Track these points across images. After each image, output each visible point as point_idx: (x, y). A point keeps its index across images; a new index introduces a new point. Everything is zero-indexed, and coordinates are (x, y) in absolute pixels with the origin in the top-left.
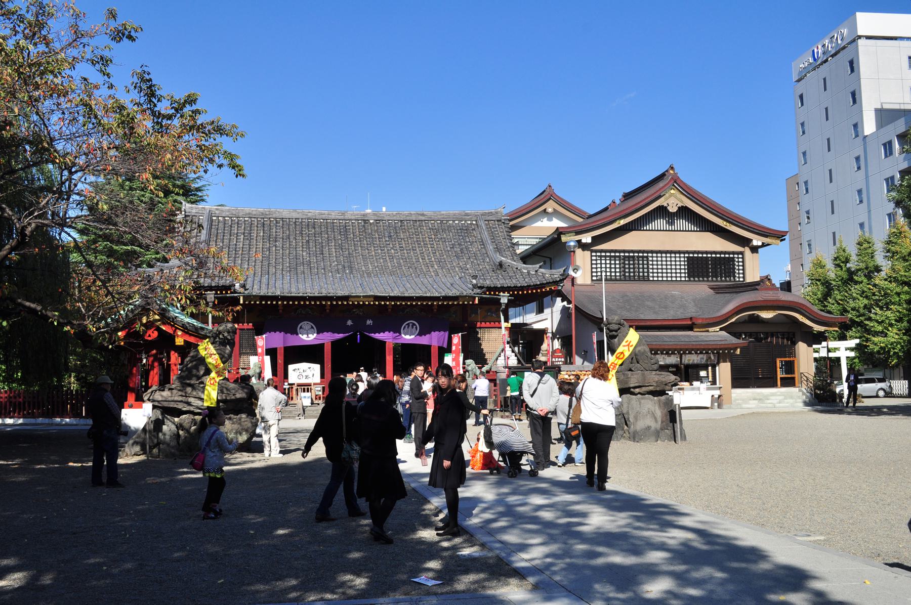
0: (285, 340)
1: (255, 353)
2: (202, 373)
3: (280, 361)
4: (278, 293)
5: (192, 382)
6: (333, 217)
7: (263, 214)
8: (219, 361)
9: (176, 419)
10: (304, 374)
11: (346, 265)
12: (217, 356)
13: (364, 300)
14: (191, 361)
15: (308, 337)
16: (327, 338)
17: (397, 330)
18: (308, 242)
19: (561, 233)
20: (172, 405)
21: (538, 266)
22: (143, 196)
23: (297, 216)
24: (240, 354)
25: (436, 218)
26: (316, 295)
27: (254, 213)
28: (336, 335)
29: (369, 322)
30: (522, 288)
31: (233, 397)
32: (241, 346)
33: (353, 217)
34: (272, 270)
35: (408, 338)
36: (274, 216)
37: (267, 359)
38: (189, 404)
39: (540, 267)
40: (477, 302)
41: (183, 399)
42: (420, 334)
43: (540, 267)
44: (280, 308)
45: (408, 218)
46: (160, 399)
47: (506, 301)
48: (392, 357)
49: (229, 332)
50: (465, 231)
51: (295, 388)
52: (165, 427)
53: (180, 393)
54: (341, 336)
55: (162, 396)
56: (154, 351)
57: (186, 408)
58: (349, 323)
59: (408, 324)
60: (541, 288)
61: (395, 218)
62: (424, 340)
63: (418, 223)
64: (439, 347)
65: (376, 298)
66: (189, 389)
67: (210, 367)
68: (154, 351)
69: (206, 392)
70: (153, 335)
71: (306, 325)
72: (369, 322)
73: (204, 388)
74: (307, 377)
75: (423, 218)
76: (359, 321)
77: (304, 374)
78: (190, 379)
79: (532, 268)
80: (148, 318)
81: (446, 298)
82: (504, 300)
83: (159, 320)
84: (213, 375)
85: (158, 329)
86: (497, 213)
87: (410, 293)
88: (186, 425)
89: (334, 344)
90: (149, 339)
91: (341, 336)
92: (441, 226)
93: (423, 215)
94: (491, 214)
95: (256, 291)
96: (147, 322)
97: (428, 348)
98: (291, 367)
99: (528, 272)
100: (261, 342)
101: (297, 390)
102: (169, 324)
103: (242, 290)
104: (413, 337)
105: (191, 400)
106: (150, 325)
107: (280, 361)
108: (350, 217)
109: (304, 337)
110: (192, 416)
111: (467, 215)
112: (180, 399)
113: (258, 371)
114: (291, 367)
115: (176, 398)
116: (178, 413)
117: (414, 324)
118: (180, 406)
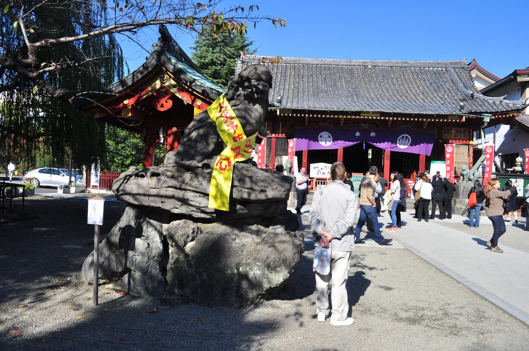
0: (309, 145)
1: (286, 154)
2: (211, 147)
3: (305, 160)
4: (306, 108)
5: (194, 163)
6: (343, 63)
7: (294, 61)
8: (240, 130)
9: (165, 226)
10: (322, 171)
11: (354, 93)
12: (237, 122)
13: (373, 115)
14: (196, 128)
15: (326, 143)
16: (340, 145)
17: (394, 141)
18: (325, 78)
19: (518, 75)
20: (156, 203)
21: (503, 97)
22: (220, 57)
23: (318, 63)
24: (276, 155)
25: (416, 65)
26: (335, 110)
27: (288, 60)
28: (347, 143)
29: (373, 134)
30: (502, 113)
31: (262, 196)
32: (276, 150)
33: (357, 64)
34: (301, 95)
35: (402, 147)
36: (302, 62)
37: (296, 158)
38: (184, 201)
39: (504, 99)
40: (464, 120)
41: (179, 194)
42: (412, 145)
43: (504, 99)
44: (307, 121)
45: (396, 65)
46: (135, 190)
47: (489, 120)
48: (389, 161)
49: (259, 79)
50: (438, 74)
51: (314, 181)
52: (139, 242)
53: (173, 182)
54: (351, 143)
55: (139, 186)
56: (174, 129)
57: (183, 210)
58: (358, 134)
59: (403, 137)
60: (506, 114)
61: (386, 65)
62: (416, 150)
63: (403, 68)
64: (426, 156)
65: (382, 114)
66: (187, 176)
67: (225, 138)
68: (174, 129)
69: (213, 181)
70: (166, 105)
71: (325, 134)
72: (373, 134)
73: (210, 174)
74: (324, 173)
75: (407, 65)
76: (365, 133)
77: (322, 171)
78: (192, 158)
79: (497, 99)
80: (162, 83)
81: (439, 116)
82: (487, 119)
83: (174, 86)
84: (227, 152)
85: (173, 97)
86: (461, 63)
87: (410, 111)
88: (179, 236)
89: (345, 149)
90: (162, 109)
91: (351, 143)
92: (420, 71)
93: (407, 63)
94: (456, 63)
95: (289, 106)
96: (162, 87)
97: (416, 157)
98: (312, 166)
99: (494, 103)
100: (292, 143)
101: (316, 182)
102: (187, 91)
103: (278, 105)
104: (406, 147)
105: (189, 195)
106: (164, 92)
107: (305, 160)
108: (354, 64)
109: (323, 143)
110: (192, 225)
111: (439, 63)
112: (171, 192)
113: (289, 166)
114: (312, 166)
115: (163, 192)
116: (167, 216)
117: (407, 137)
118: (168, 205)
